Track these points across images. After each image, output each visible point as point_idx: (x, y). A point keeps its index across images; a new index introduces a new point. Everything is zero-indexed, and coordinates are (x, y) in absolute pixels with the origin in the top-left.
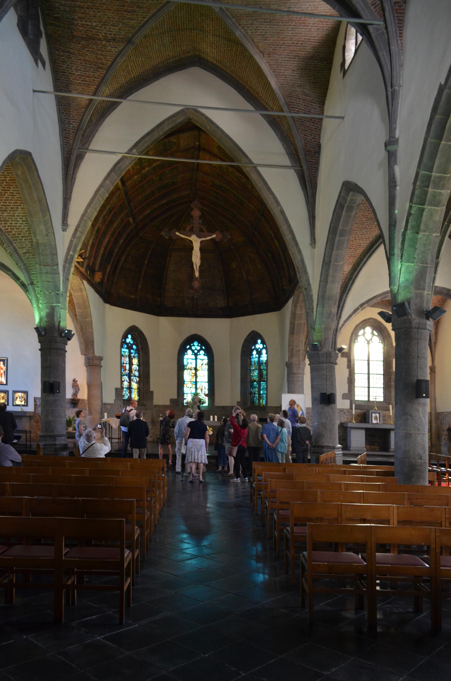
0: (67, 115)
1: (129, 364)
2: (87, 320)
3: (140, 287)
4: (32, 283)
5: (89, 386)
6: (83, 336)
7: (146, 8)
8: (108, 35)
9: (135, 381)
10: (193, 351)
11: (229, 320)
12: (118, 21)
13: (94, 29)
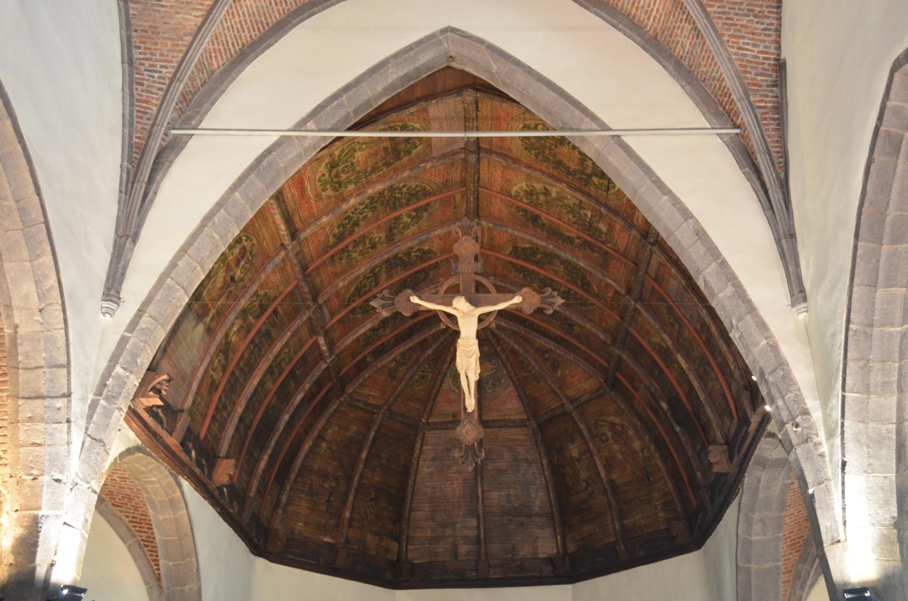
0: (148, 51)
2: (187, 587)
3: (347, 514)
11: (568, 587)
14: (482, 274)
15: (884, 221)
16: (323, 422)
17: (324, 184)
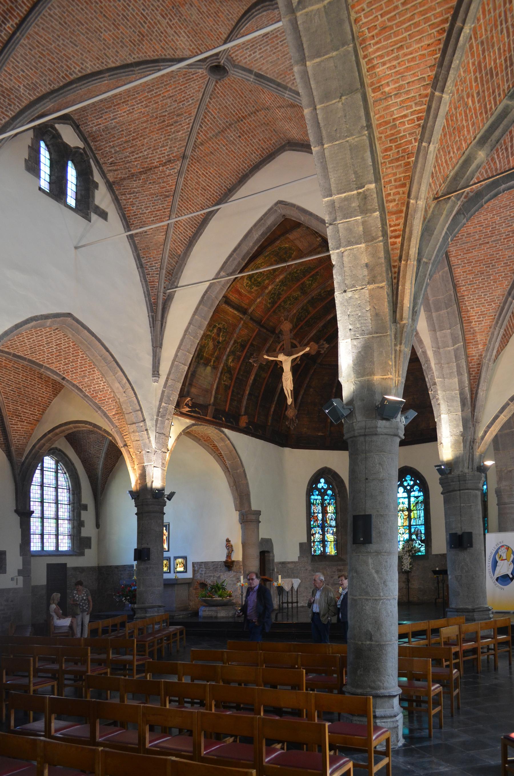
1: (322, 513)
4: (126, 445)
5: (244, 545)
6: (237, 490)
7: (185, 113)
8: (162, 159)
9: (331, 532)
10: (405, 488)
12: (166, 140)
13: (147, 158)
14: (293, 339)
15: (429, 303)
16: (308, 379)
17: (250, 286)
